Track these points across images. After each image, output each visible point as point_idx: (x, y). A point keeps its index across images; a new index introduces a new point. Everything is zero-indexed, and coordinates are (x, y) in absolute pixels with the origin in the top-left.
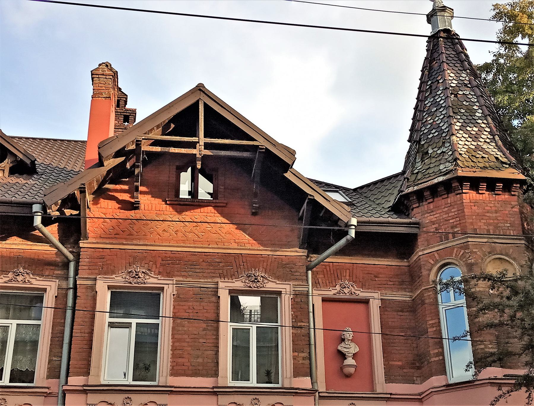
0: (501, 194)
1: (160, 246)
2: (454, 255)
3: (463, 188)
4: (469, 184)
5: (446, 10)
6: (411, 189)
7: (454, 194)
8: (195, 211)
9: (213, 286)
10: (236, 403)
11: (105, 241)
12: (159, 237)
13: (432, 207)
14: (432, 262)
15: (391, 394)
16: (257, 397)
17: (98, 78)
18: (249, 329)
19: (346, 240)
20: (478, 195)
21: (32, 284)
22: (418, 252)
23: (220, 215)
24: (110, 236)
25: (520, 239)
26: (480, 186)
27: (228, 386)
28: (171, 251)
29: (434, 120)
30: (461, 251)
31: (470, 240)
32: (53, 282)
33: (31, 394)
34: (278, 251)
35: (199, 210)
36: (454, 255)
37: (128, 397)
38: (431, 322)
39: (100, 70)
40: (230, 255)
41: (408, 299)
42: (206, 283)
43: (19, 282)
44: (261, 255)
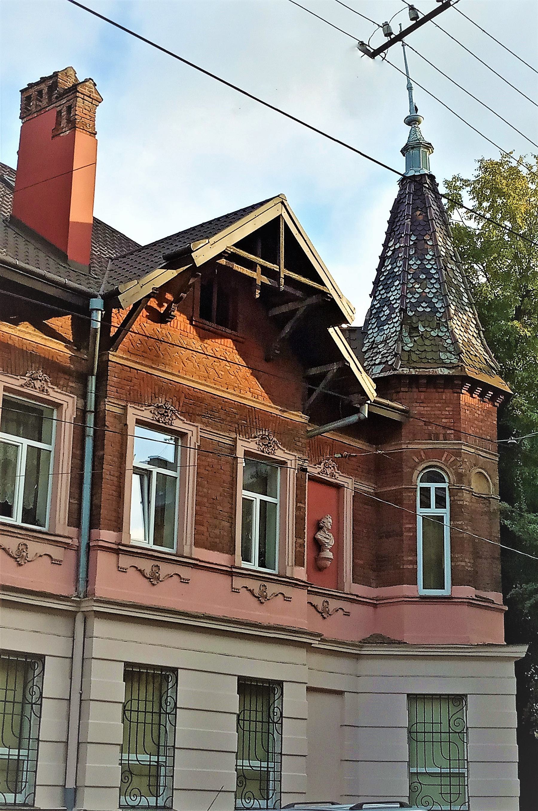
0: (486, 402)
1: (184, 378)
2: (443, 459)
3: (463, 388)
4: (481, 389)
5: (430, 149)
6: (406, 371)
7: (451, 390)
8: (217, 340)
9: (230, 443)
10: (137, 568)
11: (133, 358)
12: (184, 366)
13: (422, 397)
14: (417, 460)
15: (357, 596)
16: (266, 584)
17: (83, 99)
18: (253, 501)
19: (357, 418)
20: (471, 398)
21: (49, 395)
22: (401, 444)
23: (237, 353)
24: (138, 353)
25: (495, 455)
26: (476, 390)
27: (131, 544)
28: (194, 388)
29: (423, 290)
30: (451, 457)
31: (463, 447)
32: (70, 398)
33: (52, 543)
34: (286, 412)
35: (219, 341)
36: (443, 459)
37: (157, 565)
38: (407, 526)
39: (87, 88)
40: (246, 407)
41: (372, 491)
42: (224, 437)
43: (36, 389)
44: (271, 413)
